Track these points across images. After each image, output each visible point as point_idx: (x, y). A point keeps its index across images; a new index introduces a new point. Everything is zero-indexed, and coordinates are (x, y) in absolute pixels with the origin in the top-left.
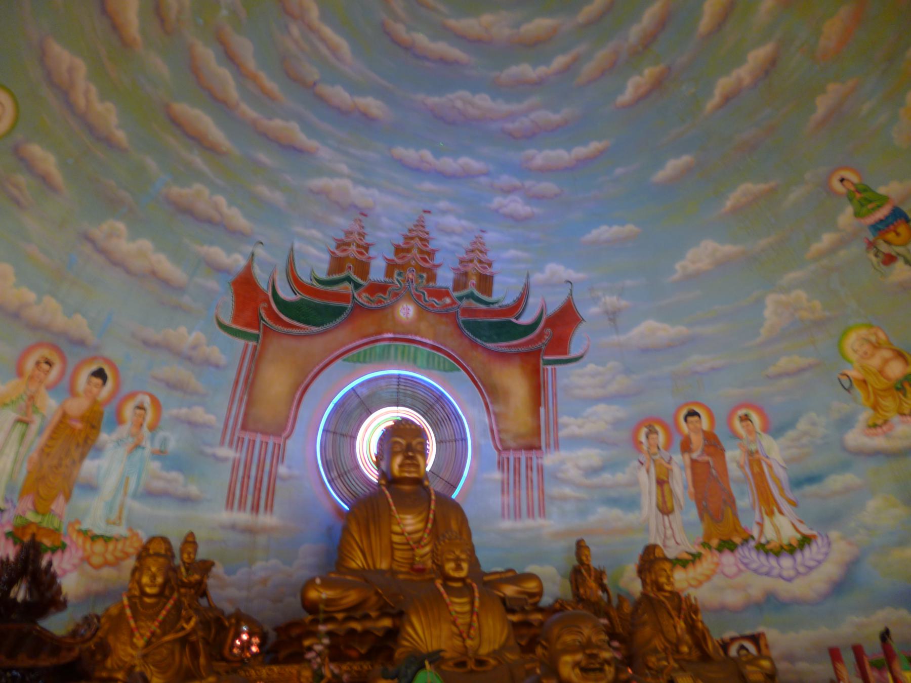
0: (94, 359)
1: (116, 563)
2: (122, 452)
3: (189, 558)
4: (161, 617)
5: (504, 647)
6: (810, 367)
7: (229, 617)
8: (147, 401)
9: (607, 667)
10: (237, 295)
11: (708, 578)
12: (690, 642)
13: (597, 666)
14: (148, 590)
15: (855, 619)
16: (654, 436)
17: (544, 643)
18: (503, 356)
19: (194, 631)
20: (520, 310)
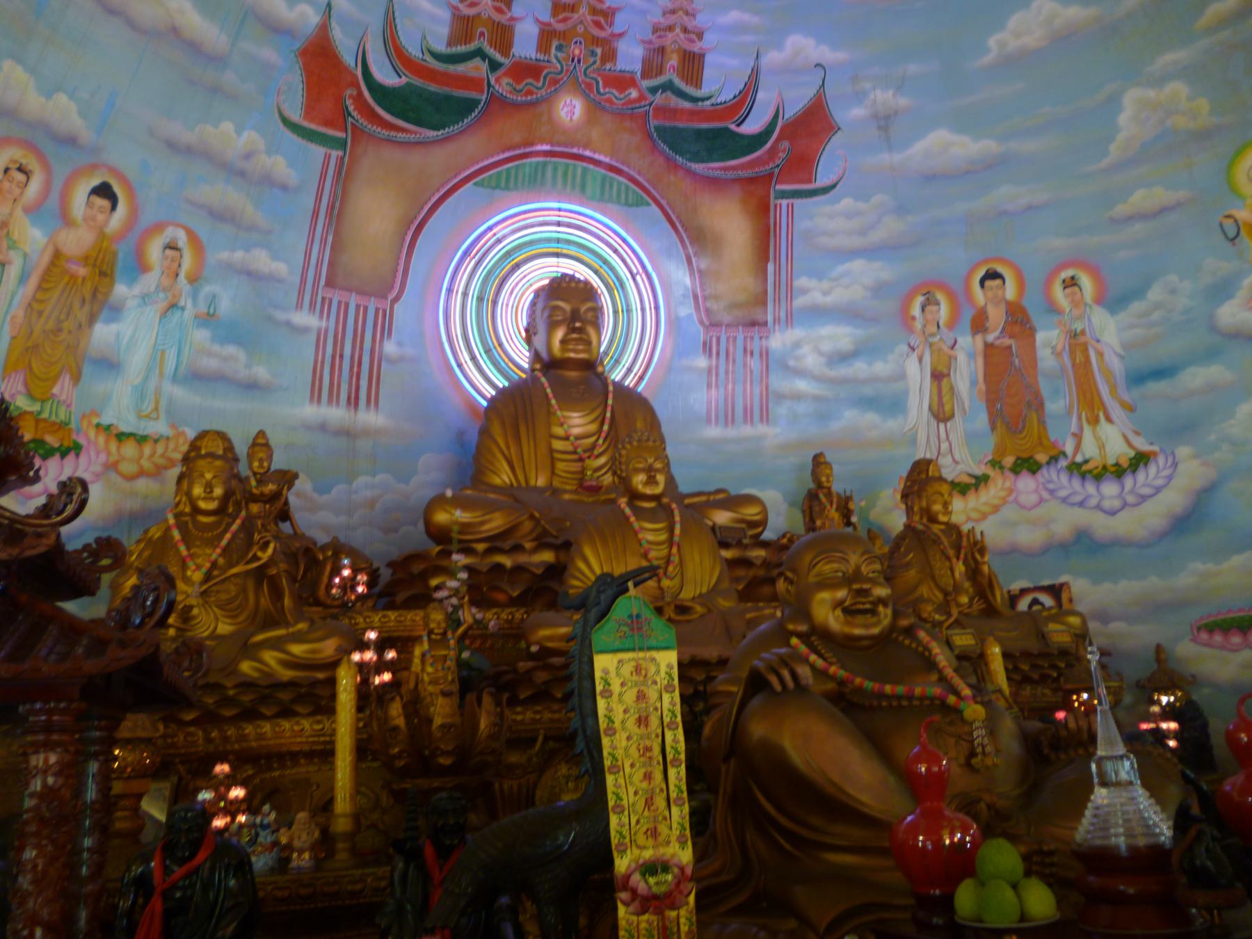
0: (94, 167)
1: (157, 473)
2: (152, 313)
3: (261, 466)
4: (224, 542)
5: (714, 590)
6: (1178, 205)
7: (324, 548)
8: (182, 238)
9: (881, 609)
10: (308, 72)
11: (996, 509)
12: (971, 590)
13: (868, 606)
14: (202, 505)
15: (1200, 566)
16: (934, 308)
17: (789, 574)
18: (714, 184)
19: (271, 561)
20: (744, 110)
